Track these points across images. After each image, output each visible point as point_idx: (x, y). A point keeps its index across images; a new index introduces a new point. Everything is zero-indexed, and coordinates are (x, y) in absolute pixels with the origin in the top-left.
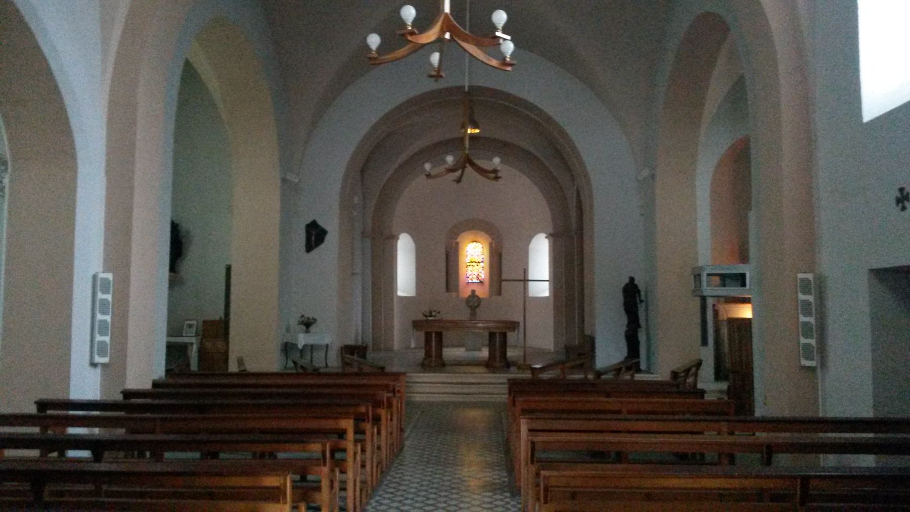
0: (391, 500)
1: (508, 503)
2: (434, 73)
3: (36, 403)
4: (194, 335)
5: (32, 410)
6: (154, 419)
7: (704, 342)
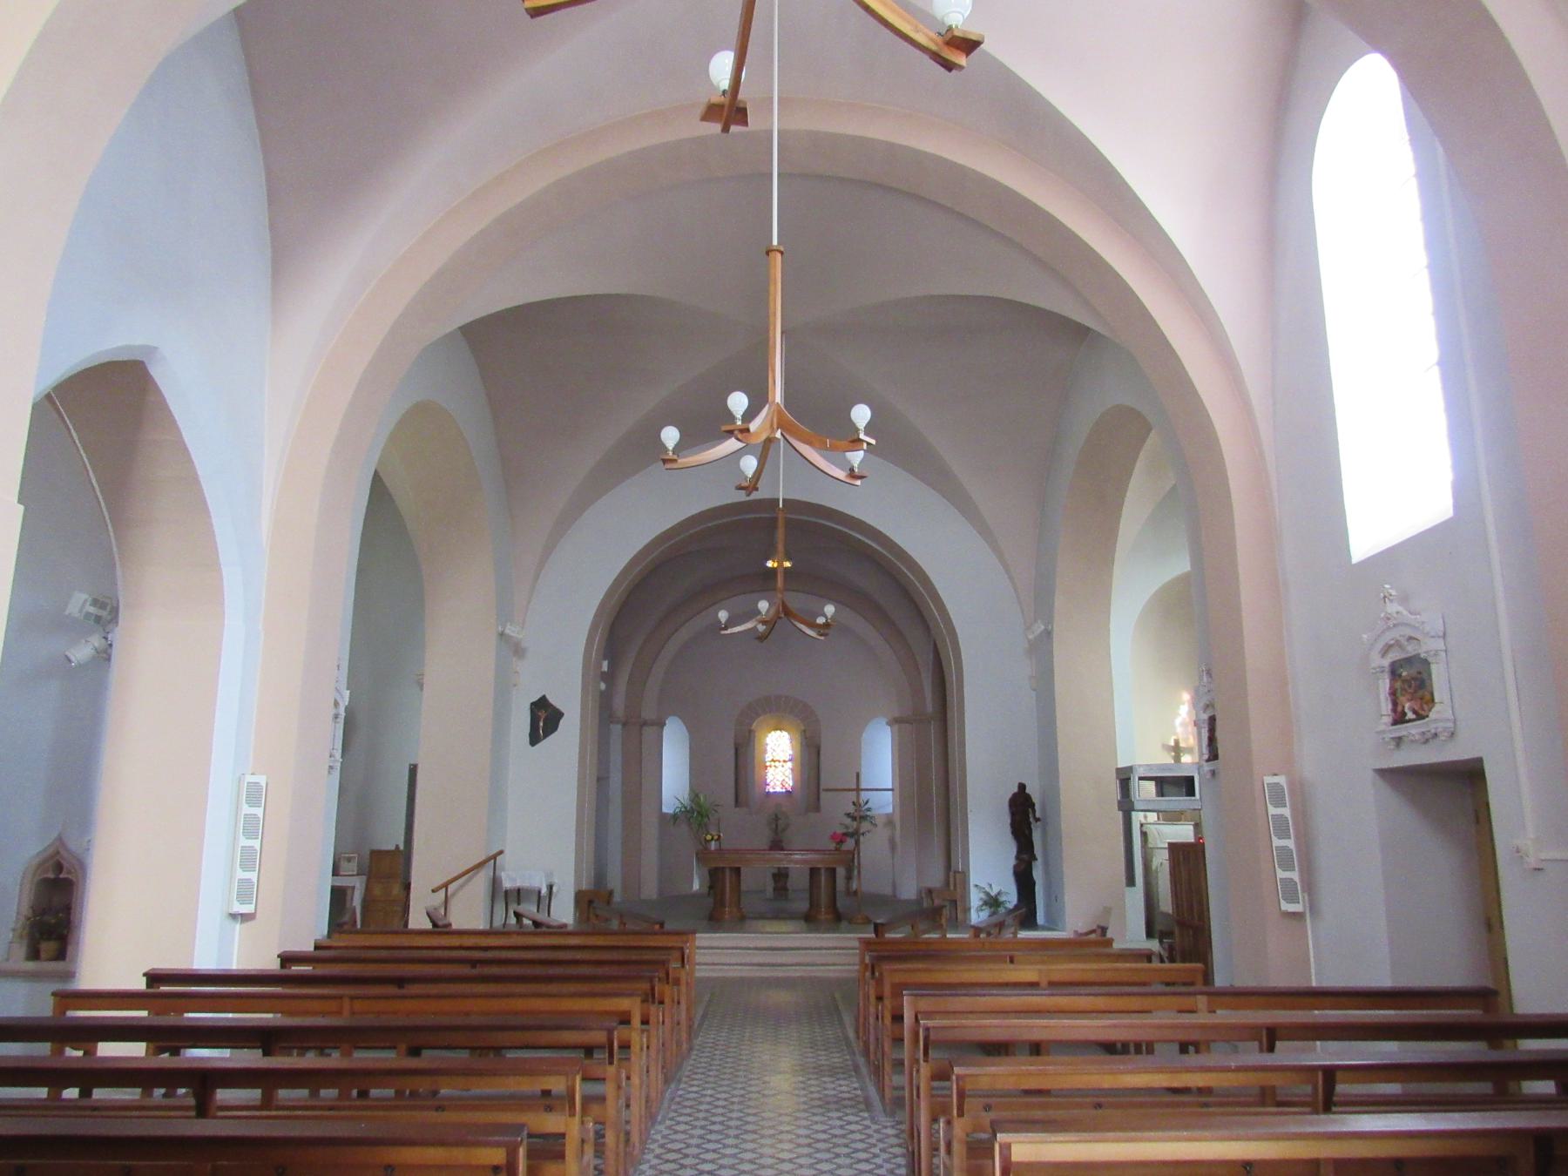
0: (691, 1125)
1: (867, 1127)
2: (745, 484)
3: (145, 975)
4: (355, 873)
5: (140, 984)
6: (341, 997)
7: (1131, 881)
